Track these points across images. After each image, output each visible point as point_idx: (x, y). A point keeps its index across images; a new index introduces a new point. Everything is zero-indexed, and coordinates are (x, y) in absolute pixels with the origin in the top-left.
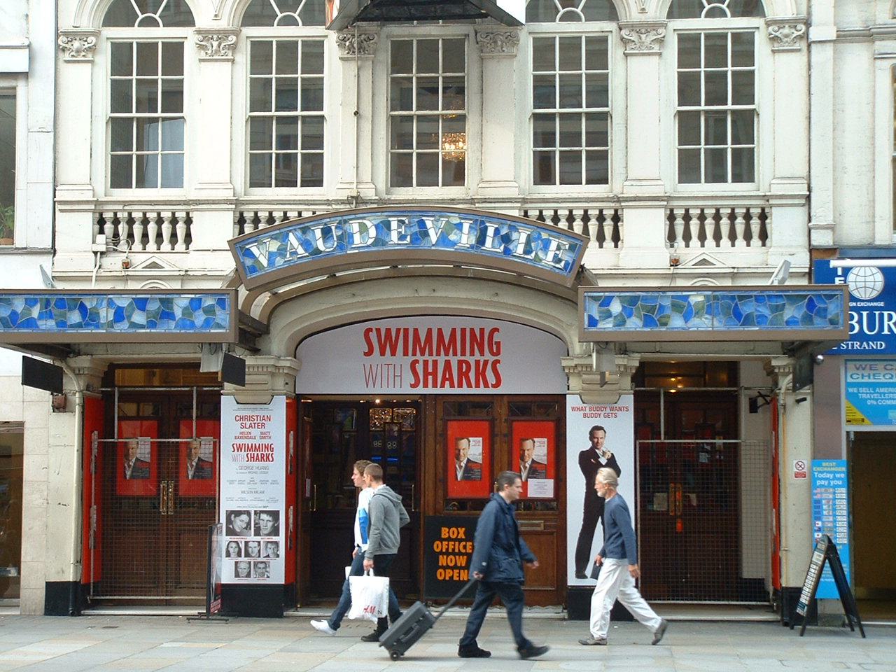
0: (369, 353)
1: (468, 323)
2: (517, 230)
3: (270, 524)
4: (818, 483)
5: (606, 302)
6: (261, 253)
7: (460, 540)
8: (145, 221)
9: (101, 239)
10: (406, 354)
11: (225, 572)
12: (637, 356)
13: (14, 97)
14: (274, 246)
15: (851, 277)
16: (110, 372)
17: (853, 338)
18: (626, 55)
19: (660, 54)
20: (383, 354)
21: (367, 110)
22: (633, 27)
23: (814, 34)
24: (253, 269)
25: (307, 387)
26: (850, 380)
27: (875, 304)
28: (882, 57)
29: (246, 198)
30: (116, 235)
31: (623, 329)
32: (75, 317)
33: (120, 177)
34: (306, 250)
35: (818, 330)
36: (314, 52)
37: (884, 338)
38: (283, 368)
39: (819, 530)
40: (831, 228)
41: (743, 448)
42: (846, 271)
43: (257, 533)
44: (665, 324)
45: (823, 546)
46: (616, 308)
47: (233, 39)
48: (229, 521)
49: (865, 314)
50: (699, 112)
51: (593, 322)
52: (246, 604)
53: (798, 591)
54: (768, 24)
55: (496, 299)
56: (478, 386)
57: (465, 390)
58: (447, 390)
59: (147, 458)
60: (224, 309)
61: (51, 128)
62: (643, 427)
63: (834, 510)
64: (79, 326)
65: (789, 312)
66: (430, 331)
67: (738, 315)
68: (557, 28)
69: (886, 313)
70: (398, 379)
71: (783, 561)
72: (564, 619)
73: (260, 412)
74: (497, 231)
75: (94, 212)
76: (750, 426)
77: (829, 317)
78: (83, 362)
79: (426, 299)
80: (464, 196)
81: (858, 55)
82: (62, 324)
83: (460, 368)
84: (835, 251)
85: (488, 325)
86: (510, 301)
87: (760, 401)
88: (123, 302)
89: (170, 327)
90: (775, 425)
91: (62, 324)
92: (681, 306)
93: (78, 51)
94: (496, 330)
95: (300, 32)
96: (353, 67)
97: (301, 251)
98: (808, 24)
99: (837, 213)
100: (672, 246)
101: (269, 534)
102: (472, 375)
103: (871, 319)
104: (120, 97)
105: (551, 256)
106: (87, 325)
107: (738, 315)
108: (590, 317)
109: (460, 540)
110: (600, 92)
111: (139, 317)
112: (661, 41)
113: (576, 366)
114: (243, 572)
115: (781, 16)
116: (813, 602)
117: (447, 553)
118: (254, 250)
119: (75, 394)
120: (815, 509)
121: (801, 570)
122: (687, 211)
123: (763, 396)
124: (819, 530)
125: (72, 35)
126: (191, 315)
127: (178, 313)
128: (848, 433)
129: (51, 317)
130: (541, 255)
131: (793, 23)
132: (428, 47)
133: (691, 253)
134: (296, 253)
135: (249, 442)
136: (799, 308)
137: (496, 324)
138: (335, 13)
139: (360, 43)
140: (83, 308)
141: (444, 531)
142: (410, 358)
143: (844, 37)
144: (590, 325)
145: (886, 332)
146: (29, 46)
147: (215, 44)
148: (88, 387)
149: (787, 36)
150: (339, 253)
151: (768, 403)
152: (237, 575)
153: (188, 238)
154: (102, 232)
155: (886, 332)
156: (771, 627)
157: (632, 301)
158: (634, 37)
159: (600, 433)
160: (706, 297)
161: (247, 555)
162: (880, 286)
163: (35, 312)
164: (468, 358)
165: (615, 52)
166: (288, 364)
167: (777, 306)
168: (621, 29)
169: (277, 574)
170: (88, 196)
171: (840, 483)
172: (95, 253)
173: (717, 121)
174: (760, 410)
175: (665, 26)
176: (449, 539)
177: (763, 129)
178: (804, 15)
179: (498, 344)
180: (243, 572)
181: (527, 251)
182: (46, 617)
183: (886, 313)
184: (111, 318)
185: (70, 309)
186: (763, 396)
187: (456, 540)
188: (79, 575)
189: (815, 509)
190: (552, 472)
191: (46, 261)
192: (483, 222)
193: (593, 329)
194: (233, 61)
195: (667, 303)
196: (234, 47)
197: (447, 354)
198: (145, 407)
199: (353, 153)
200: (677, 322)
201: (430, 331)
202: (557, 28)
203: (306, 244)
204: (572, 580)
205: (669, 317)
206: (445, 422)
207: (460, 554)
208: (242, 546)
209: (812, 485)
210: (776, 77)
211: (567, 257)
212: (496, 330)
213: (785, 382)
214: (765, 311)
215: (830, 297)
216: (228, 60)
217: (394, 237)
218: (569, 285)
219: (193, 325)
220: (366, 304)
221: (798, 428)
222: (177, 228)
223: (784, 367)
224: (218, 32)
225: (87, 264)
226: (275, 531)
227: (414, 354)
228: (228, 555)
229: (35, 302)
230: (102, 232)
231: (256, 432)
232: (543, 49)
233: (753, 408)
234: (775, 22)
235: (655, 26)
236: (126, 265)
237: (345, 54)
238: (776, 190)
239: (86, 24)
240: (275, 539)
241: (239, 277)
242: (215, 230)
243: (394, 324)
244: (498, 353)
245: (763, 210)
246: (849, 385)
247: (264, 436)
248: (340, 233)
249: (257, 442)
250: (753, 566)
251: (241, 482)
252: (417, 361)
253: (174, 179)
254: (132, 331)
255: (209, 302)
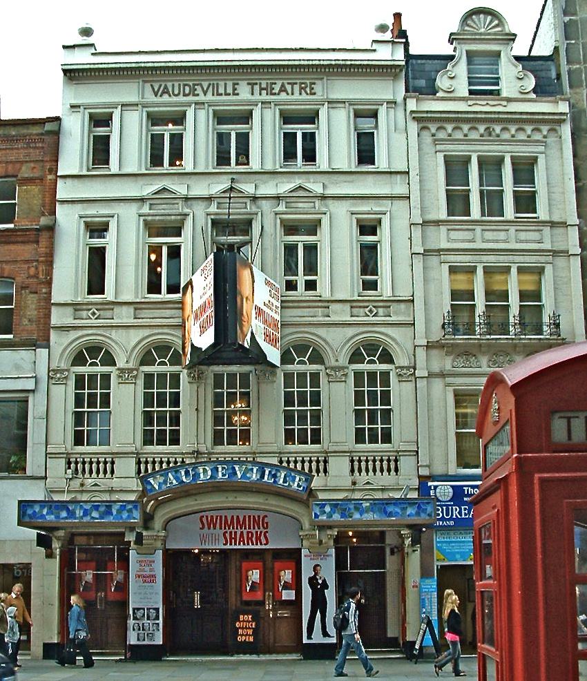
0: (203, 528)
1: (252, 513)
2: (280, 472)
3: (155, 614)
4: (424, 590)
5: (323, 506)
6: (155, 483)
7: (249, 622)
8: (91, 463)
9: (69, 471)
10: (221, 528)
11: (132, 639)
12: (336, 529)
13: (27, 401)
14: (161, 480)
15: (438, 490)
16: (70, 540)
17: (439, 520)
18: (329, 382)
19: (345, 381)
20: (209, 528)
21: (201, 408)
22: (332, 368)
23: (418, 373)
24: (151, 490)
25: (172, 545)
26: (438, 540)
27: (449, 503)
28: (449, 385)
29: (142, 451)
30: (76, 469)
31: (331, 519)
32: (64, 514)
33: (78, 440)
34: (177, 482)
35: (423, 519)
36: (175, 378)
37: (453, 519)
38: (161, 536)
39: (424, 613)
40: (428, 466)
41: (388, 576)
42: (436, 487)
43: (148, 619)
44: (351, 517)
45: (425, 621)
46: (328, 509)
47: (135, 372)
48: (134, 613)
49: (444, 508)
50: (364, 409)
51: (316, 516)
52: (144, 654)
53: (414, 643)
54: (396, 368)
55: (266, 502)
56: (257, 544)
57: (251, 547)
58: (242, 546)
59: (91, 581)
60: (137, 510)
61: (45, 417)
62: (340, 564)
63: (431, 603)
64: (66, 518)
65: (410, 511)
66: (233, 517)
67: (385, 512)
68: (294, 368)
69: (454, 508)
70: (217, 541)
71: (407, 628)
72: (301, 660)
73: (150, 558)
74: (270, 472)
75: (66, 458)
76: (391, 562)
77: (428, 513)
78: (61, 533)
79: (232, 502)
80: (249, 451)
81: (438, 384)
82: (58, 517)
83: (248, 536)
84: (431, 478)
85: (262, 514)
86: (274, 503)
87: (396, 550)
88: (88, 507)
89: (111, 519)
90: (403, 563)
91: (58, 517)
92: (358, 508)
93: (59, 379)
94: (266, 516)
95: (169, 369)
96: (195, 386)
97: (174, 482)
98: (415, 369)
99: (431, 459)
100: (353, 475)
101: (154, 620)
102: (254, 539)
103: (447, 510)
104: (79, 401)
105: (296, 484)
106: (70, 518)
107: (385, 512)
108: (315, 513)
109: (249, 622)
110: (316, 399)
111: (95, 514)
112: (345, 375)
113: (306, 535)
114: (141, 639)
115: (402, 365)
116: (421, 647)
117: (243, 628)
118: (152, 482)
119: (56, 549)
120: (422, 603)
121: (416, 634)
122: (360, 458)
123: (397, 548)
124: (424, 613)
125: (56, 371)
126: (120, 513)
127: (114, 512)
128: (437, 566)
129: (52, 514)
130: (291, 484)
131: (408, 368)
132: (232, 376)
133: (363, 478)
134: (172, 483)
135: (144, 573)
136: (414, 509)
137: (266, 513)
138: (188, 362)
139: (198, 375)
140: (68, 510)
141: (241, 616)
142: (223, 531)
143: (431, 375)
144: (315, 517)
145: (454, 517)
146: (35, 377)
147: (127, 375)
148: (62, 546)
149: (405, 374)
150: (193, 483)
151: (399, 551)
152: (138, 640)
153: (112, 472)
154: (69, 468)
155: (454, 517)
156: (402, 661)
157: (335, 505)
158: (333, 373)
159: (319, 568)
160: (371, 504)
161: (143, 630)
162: (451, 495)
163: (45, 512)
164: (252, 530)
165: (323, 380)
166: (163, 534)
167: (404, 508)
168: (326, 369)
169: (159, 641)
170: (63, 450)
171: (434, 590)
172: (67, 479)
173: (372, 414)
174: (396, 554)
175: (347, 368)
176: (244, 621)
177: (395, 417)
178: (412, 365)
179: (267, 523)
180: (141, 639)
181: (285, 481)
182: (45, 660)
183: (454, 508)
184: (82, 514)
185: (62, 510)
186: (397, 548)
187: (247, 621)
188: (60, 639)
189: (422, 603)
190: (294, 587)
191: (41, 483)
192: (263, 468)
193: (317, 519)
194: (135, 383)
195: (352, 507)
196: (135, 377)
197: (241, 528)
198: (89, 553)
199: (194, 430)
200: (357, 516)
201: (233, 517)
202: (294, 368)
203: (176, 478)
204: (305, 641)
205: (353, 513)
206: (241, 563)
207: (249, 628)
208: (141, 625)
209: (420, 593)
210: (400, 391)
211: (304, 485)
212: (266, 516)
213: (408, 542)
214: (399, 511)
215: (428, 503)
216: (133, 383)
217: (220, 474)
218: (305, 498)
219: (122, 517)
220: (202, 504)
221: (414, 561)
222: (108, 466)
223: (407, 534)
224: (128, 369)
225: (63, 484)
226: (157, 618)
227: (225, 528)
228: (134, 630)
229: (44, 507)
230: (69, 468)
231: (147, 568)
232: (288, 377)
233: (392, 553)
234: (400, 367)
235: (343, 368)
236: (82, 485)
237: (191, 380)
238: (120, 450)
239: (63, 366)
240: (157, 622)
241: (144, 493)
242: (126, 467)
243: (214, 513)
244: (267, 528)
245: (396, 458)
246: (437, 542)
247: (151, 570)
248: (193, 473)
249: (148, 573)
250: (392, 632)
251: (140, 593)
252: (226, 532)
253: (106, 441)
254: (92, 521)
255: (130, 507)
